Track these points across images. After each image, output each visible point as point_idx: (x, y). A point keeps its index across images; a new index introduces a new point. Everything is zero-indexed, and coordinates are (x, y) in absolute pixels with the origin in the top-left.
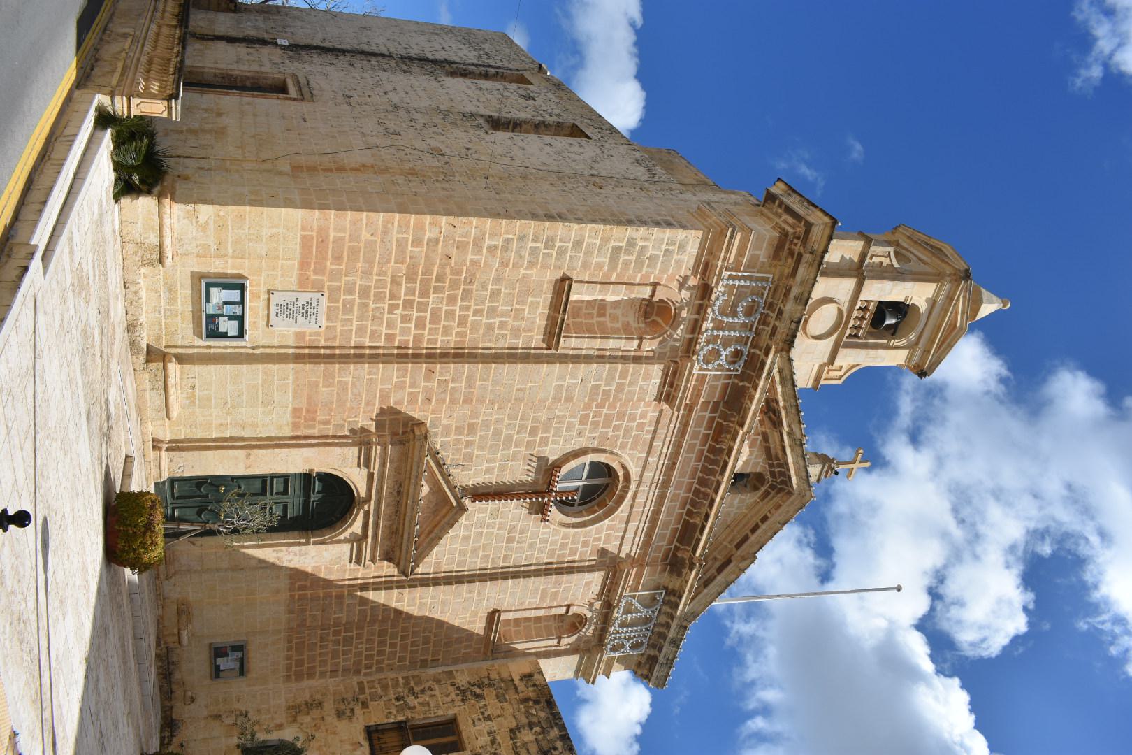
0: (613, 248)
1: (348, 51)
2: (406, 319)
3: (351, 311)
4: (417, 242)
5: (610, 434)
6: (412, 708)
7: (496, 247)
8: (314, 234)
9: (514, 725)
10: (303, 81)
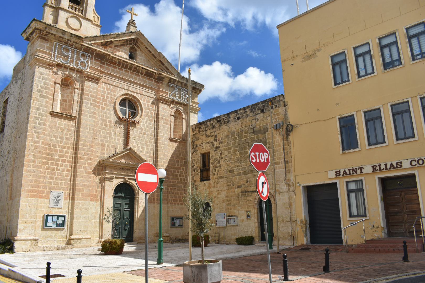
2: (62, 166)
4: (34, 162)
7: (37, 136)
9: (205, 136)
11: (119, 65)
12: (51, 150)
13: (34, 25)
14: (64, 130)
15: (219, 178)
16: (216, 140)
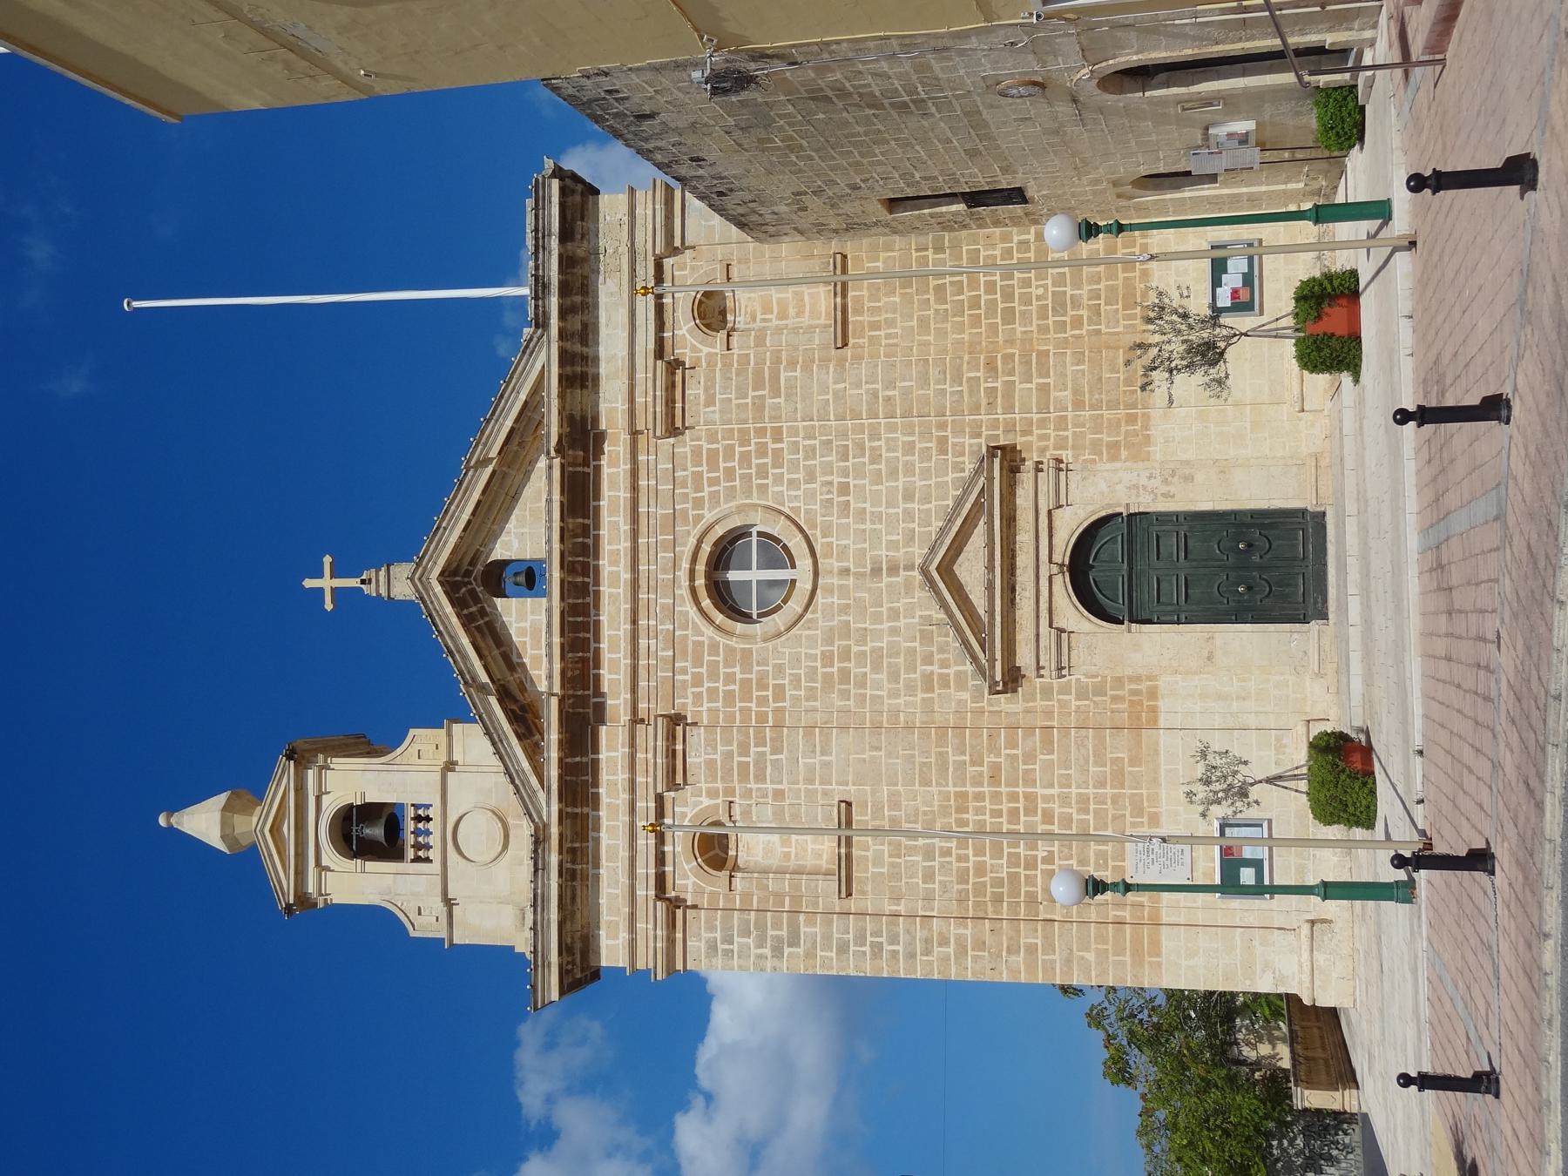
0: (797, 944)
4: (1032, 950)
5: (737, 669)
7: (940, 945)
11: (583, 645)
12: (980, 889)
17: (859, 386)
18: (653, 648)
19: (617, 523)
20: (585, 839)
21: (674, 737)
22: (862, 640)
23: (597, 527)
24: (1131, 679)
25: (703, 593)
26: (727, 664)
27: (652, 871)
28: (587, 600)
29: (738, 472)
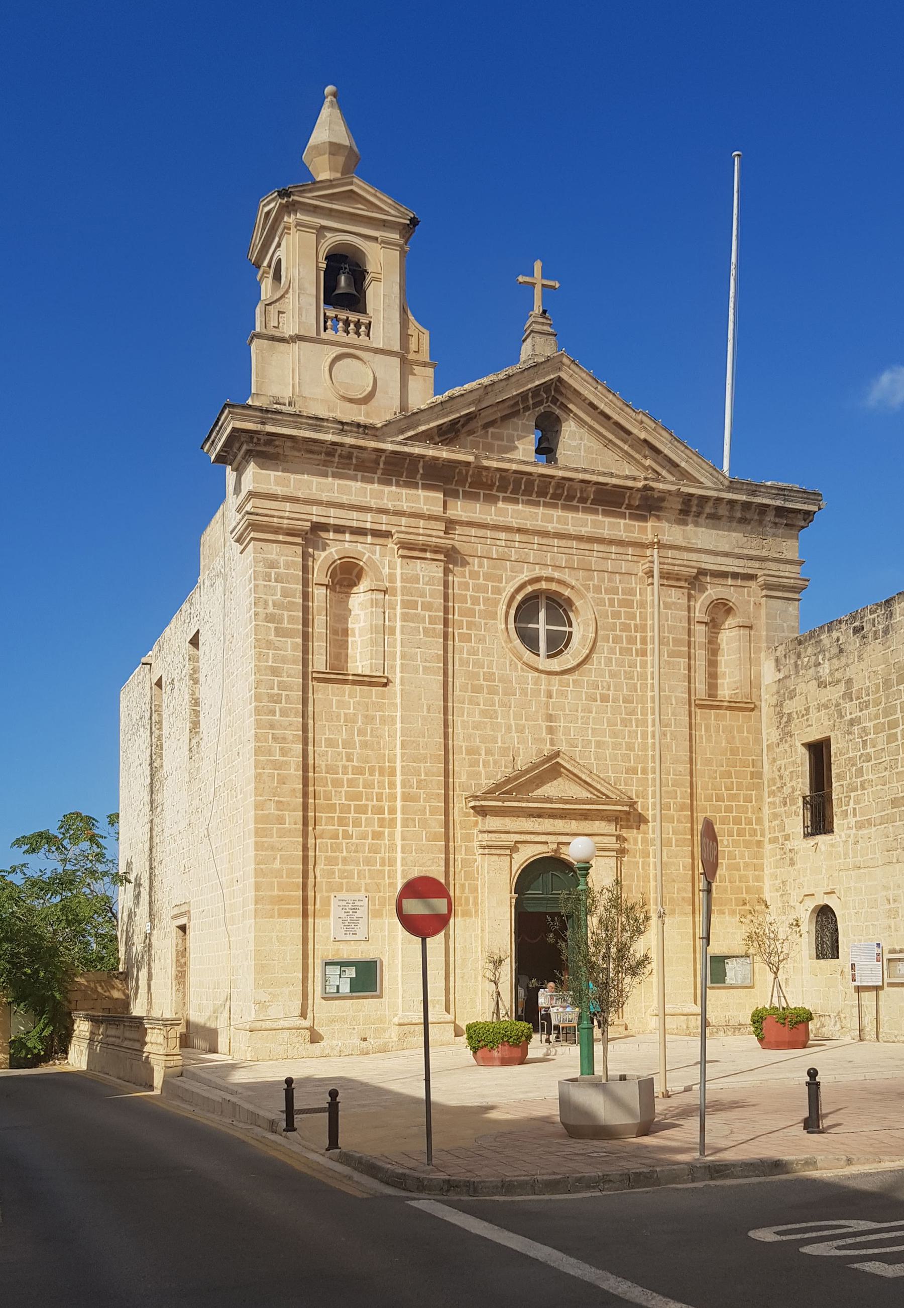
0: (277, 635)
1: (151, 864)
2: (357, 823)
3: (352, 871)
4: (281, 820)
5: (482, 607)
6: (794, 789)
7: (281, 749)
8: (276, 907)
9: (815, 683)
10: (176, 911)
11: (503, 488)
13: (230, 424)
14: (355, 722)
15: (860, 826)
16: (848, 696)
17: (673, 714)
18: (498, 542)
19: (586, 526)
20: (357, 468)
21: (436, 552)
22: (503, 704)
23: (585, 510)
24: (476, 898)
25: (536, 586)
26: (486, 600)
27: (332, 521)
28: (534, 495)
29: (618, 621)
